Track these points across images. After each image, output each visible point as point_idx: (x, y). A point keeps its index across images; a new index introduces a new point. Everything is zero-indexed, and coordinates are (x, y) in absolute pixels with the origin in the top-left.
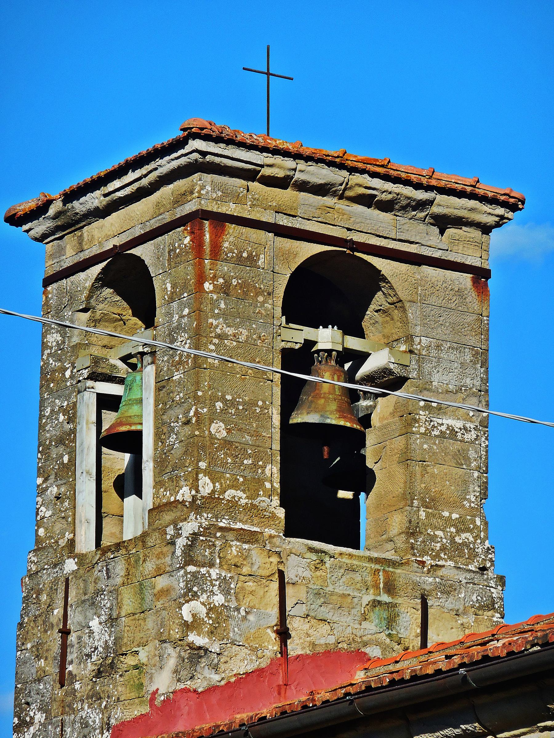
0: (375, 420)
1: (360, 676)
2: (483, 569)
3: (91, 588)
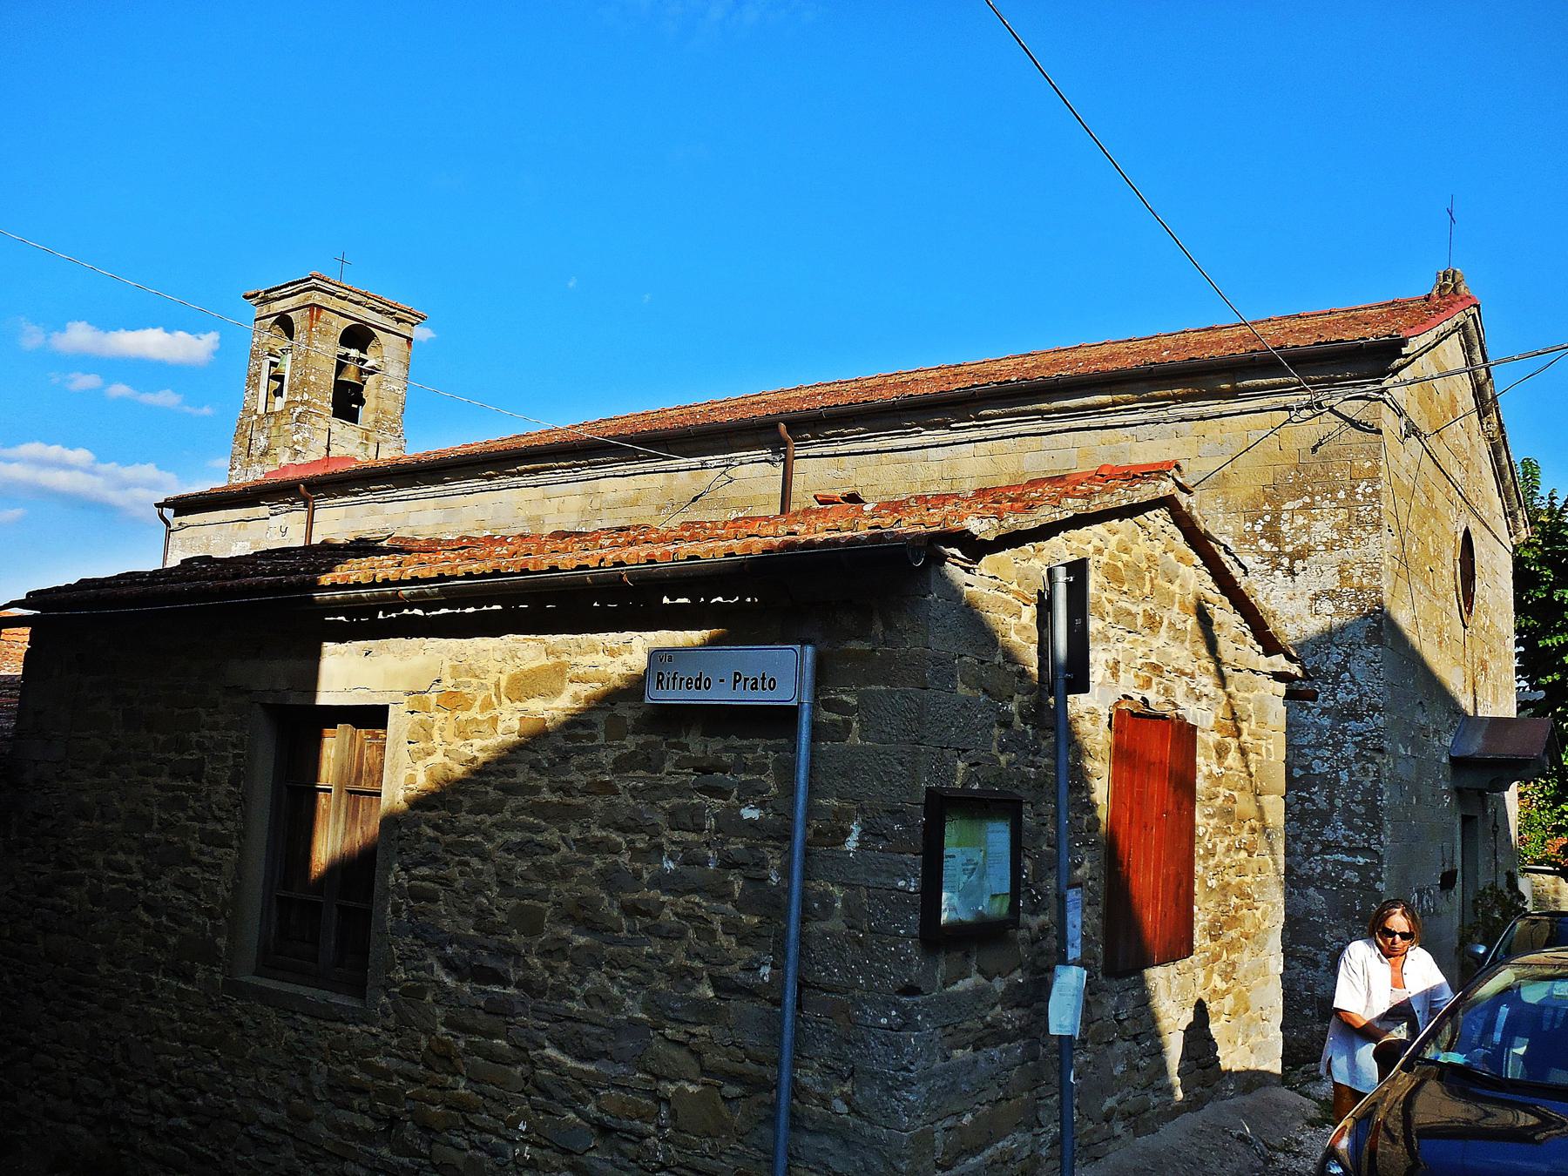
0: (367, 382)
1: (354, 466)
2: (399, 436)
3: (261, 426)
